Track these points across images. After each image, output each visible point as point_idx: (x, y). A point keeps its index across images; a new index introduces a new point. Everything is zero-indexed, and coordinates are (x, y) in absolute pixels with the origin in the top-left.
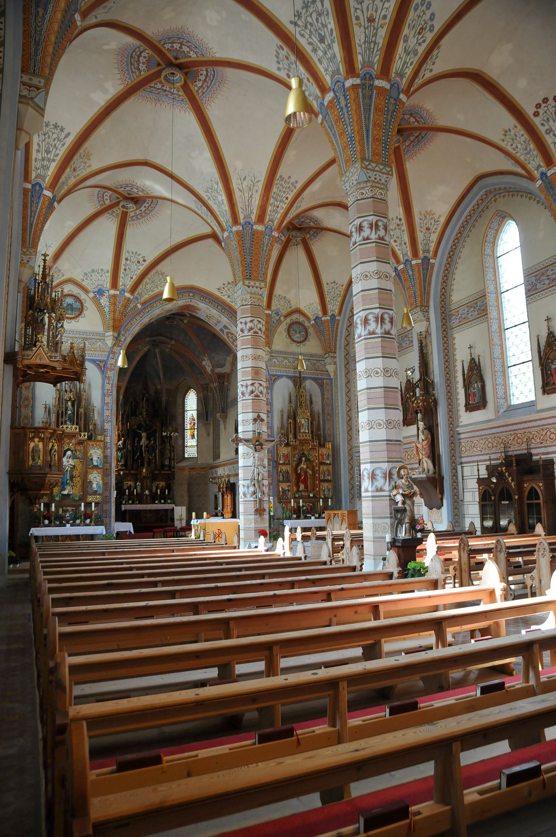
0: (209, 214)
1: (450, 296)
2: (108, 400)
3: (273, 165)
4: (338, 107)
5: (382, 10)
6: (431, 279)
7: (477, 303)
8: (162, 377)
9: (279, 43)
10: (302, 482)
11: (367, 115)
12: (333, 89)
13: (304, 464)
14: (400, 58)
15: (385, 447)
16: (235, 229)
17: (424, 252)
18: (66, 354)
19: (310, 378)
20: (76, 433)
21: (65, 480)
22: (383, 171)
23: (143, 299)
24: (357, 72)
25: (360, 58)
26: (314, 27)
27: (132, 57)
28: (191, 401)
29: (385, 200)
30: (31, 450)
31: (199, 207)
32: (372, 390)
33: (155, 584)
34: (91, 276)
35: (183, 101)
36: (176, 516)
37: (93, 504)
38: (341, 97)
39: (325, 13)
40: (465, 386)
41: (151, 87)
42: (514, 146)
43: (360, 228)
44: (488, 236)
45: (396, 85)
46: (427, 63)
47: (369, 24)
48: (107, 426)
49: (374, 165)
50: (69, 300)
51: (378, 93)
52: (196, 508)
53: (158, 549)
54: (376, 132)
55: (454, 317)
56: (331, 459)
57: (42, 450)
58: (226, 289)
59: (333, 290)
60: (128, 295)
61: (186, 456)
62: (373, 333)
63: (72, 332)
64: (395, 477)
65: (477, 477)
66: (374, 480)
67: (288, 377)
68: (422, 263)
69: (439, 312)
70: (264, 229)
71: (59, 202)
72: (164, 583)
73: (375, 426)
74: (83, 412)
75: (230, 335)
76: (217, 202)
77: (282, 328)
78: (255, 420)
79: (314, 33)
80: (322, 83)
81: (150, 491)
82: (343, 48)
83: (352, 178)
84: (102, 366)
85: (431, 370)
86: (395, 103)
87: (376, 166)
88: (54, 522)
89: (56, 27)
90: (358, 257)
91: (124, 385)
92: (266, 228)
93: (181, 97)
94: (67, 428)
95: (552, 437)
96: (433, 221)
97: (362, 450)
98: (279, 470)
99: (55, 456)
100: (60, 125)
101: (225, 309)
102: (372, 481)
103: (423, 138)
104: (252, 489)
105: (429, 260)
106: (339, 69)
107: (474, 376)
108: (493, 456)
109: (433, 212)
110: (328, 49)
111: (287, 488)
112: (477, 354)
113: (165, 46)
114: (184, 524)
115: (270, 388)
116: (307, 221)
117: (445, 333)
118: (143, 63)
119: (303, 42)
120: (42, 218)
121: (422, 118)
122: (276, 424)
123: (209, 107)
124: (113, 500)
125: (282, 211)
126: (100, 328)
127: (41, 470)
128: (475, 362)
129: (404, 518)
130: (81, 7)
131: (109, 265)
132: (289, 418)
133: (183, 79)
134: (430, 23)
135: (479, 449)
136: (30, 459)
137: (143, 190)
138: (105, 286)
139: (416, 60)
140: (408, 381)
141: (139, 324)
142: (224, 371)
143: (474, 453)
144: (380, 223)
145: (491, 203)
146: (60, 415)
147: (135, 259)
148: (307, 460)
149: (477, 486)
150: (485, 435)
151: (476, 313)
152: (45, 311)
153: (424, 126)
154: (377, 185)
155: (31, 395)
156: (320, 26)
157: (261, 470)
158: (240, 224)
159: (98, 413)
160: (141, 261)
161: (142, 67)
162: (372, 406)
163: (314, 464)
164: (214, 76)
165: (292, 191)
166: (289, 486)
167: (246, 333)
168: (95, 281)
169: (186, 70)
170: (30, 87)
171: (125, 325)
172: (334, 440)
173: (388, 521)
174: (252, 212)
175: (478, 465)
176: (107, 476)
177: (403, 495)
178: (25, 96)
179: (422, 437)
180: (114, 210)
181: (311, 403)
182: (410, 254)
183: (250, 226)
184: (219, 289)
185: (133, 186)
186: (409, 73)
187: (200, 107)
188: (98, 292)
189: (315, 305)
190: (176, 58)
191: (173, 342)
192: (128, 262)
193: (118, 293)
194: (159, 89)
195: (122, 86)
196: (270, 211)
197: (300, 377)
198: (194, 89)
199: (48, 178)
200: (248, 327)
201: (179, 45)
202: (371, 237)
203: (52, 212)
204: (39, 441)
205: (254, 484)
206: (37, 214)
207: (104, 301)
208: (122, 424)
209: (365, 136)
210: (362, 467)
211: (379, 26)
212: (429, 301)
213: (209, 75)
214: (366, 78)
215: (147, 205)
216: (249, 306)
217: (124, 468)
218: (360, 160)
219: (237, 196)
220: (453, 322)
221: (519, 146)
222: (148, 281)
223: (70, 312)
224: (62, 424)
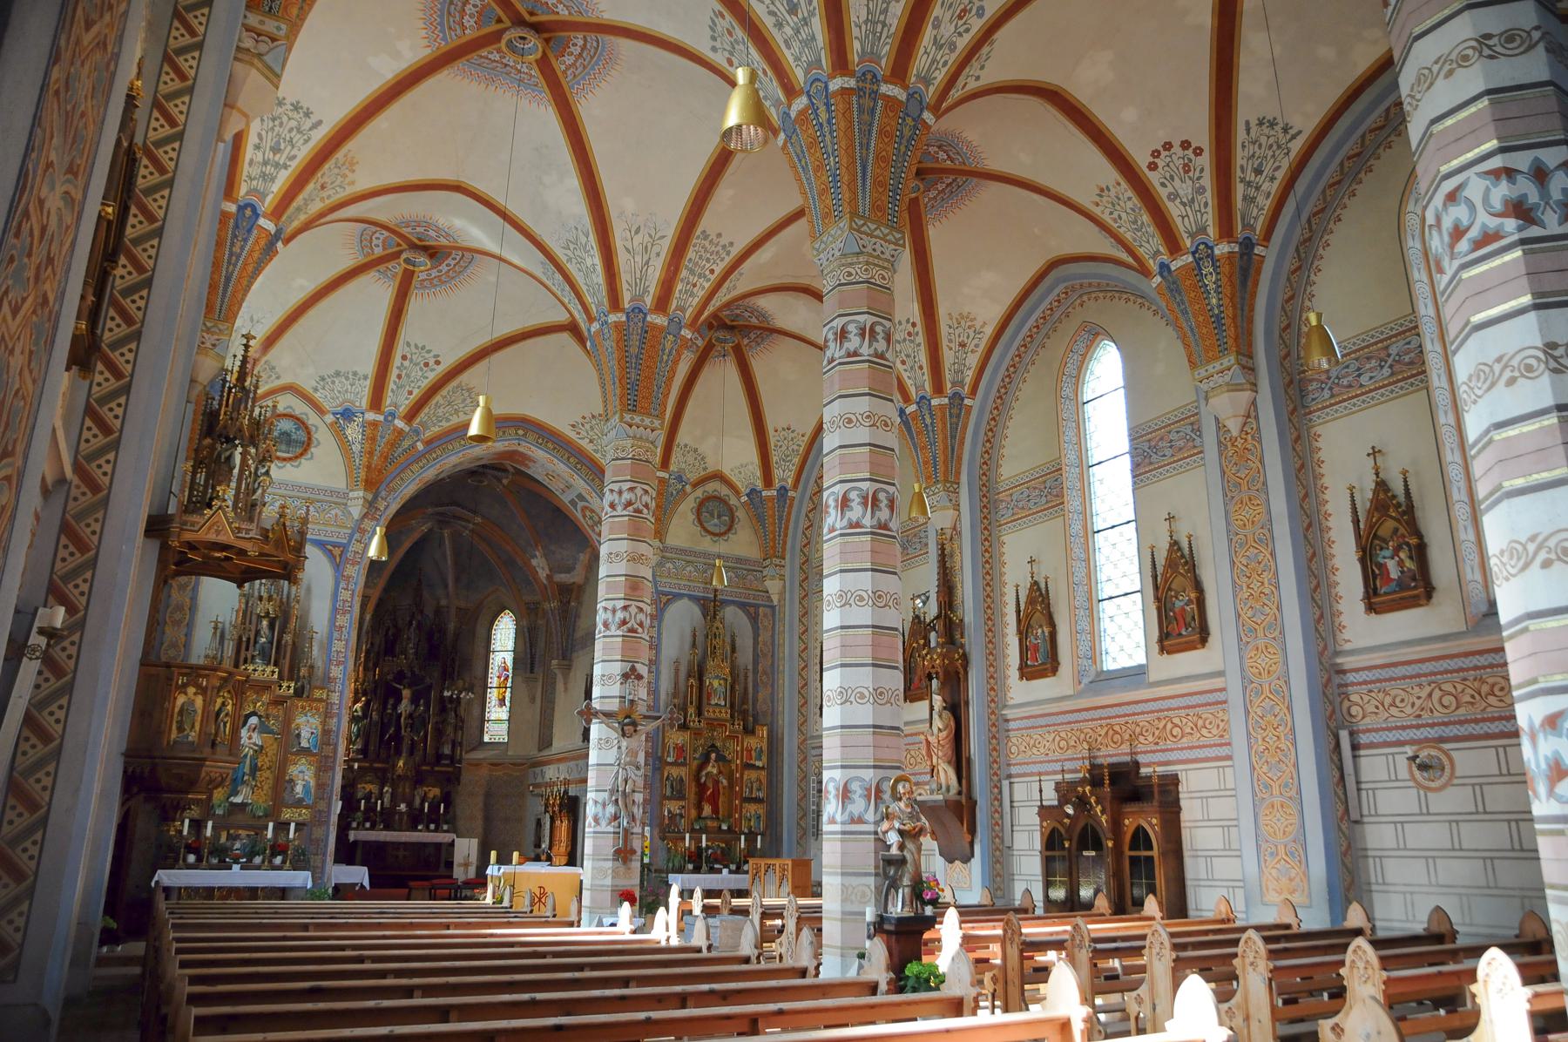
0: (567, 288)
10: (708, 801)
15: (869, 739)
16: (612, 318)
17: (954, 384)
23: (428, 434)
25: (857, 45)
28: (504, 634)
36: (458, 858)
37: (293, 826)
40: (1020, 632)
42: (1115, 215)
48: (336, 672)
50: (286, 425)
53: (417, 920)
56: (764, 758)
58: (587, 426)
60: (399, 423)
64: (887, 796)
67: (691, 597)
71: (287, 241)
77: (687, 506)
78: (625, 676)
81: (410, 805)
84: (337, 554)
91: (375, 595)
95: (1446, 700)
96: (971, 332)
104: (611, 809)
108: (1068, 766)
114: (472, 873)
118: (471, 16)
120: (250, 268)
122: (665, 685)
123: (583, 101)
124: (334, 819)
126: (340, 483)
128: (1039, 589)
129: (901, 877)
131: (369, 367)
132: (689, 676)
143: (1034, 758)
144: (878, 329)
148: (721, 758)
149: (1037, 820)
158: (623, 310)
159: (321, 647)
160: (431, 362)
161: (469, 22)
162: (848, 660)
169: (546, 35)
170: (259, 35)
173: (871, 881)
174: (646, 290)
177: (901, 832)
182: (928, 386)
185: (428, 225)
190: (532, 14)
191: (479, 520)
192: (406, 363)
193: (381, 418)
195: (428, 51)
198: (559, 66)
207: (353, 432)
210: (826, 775)
219: (622, 259)
221: (1124, 215)
223: (283, 447)
224: (245, 662)
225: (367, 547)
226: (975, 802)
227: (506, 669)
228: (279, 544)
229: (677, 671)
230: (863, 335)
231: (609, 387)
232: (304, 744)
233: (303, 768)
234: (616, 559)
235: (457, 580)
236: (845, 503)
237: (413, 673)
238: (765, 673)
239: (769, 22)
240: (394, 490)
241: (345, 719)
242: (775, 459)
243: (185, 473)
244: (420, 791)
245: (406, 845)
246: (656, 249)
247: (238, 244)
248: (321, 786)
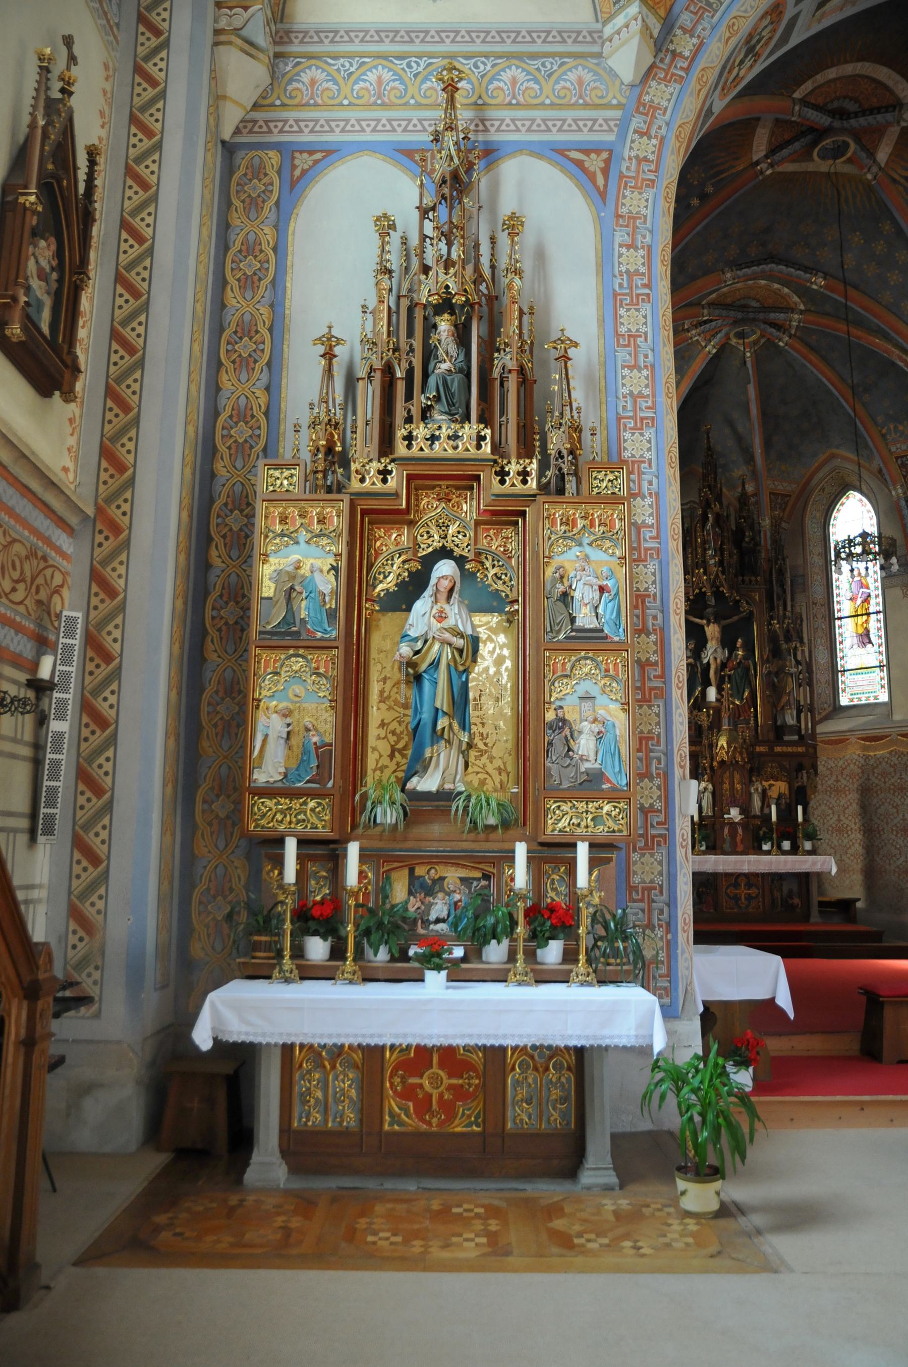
2: (631, 320)
8: (758, 451)
37: (582, 851)
48: (635, 445)
61: (844, 701)
88: (359, 954)
94: (433, 438)
146: (401, 387)
159: (590, 380)
235: (768, 444)
237: (718, 595)
244: (757, 787)
248: (643, 742)
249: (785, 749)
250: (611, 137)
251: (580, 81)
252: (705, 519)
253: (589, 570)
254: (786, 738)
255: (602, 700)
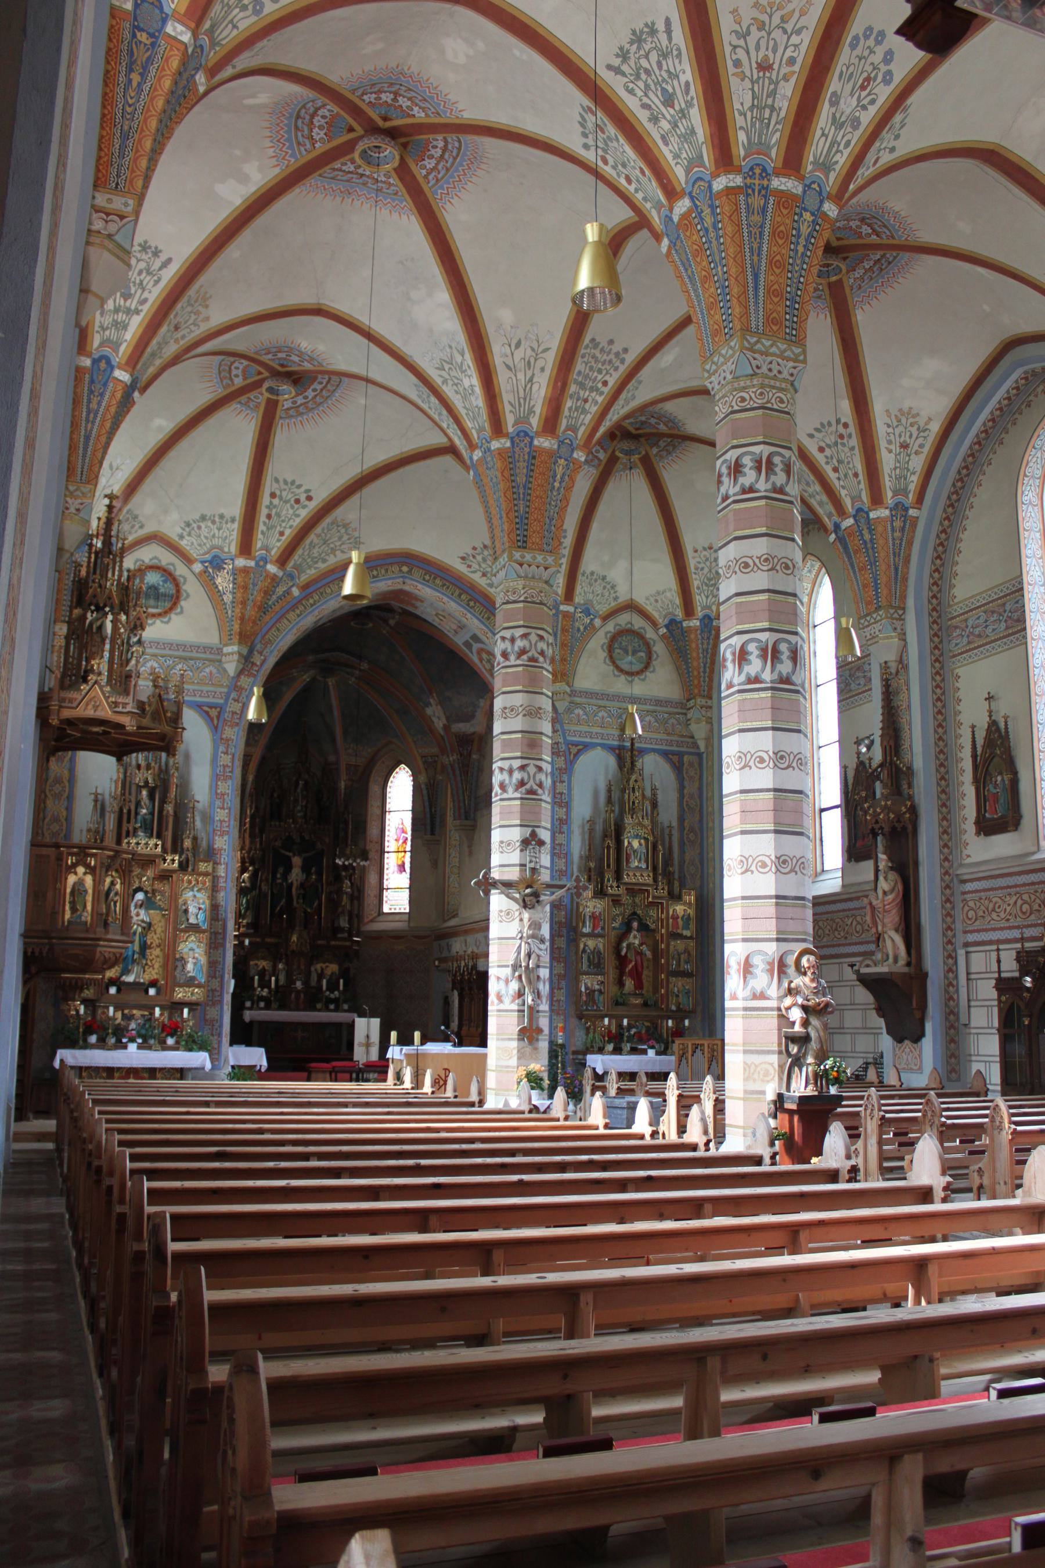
0: (445, 412)
1: (952, 586)
3: (568, 342)
4: (699, 227)
5: (786, 48)
6: (910, 550)
7: (1004, 604)
9: (587, 102)
11: (755, 246)
12: (690, 194)
13: (635, 937)
14: (823, 134)
15: (771, 911)
16: (495, 445)
17: (896, 493)
18: (145, 700)
19: (654, 750)
20: (157, 856)
21: (130, 953)
22: (786, 354)
23: (304, 578)
24: (736, 163)
25: (742, 136)
26: (653, 77)
27: (298, 117)
28: (400, 790)
29: (788, 413)
30: (68, 890)
31: (425, 396)
32: (751, 796)
33: (306, 1157)
34: (199, 528)
35: (396, 194)
36: (359, 1036)
38: (704, 208)
39: (675, 53)
40: (976, 781)
41: (334, 170)
43: (737, 469)
44: (1031, 464)
45: (815, 186)
46: (883, 139)
47: (761, 74)
49: (768, 343)
50: (152, 578)
51: (779, 203)
52: (401, 1024)
53: (318, 1100)
54: (772, 278)
55: (958, 631)
56: (692, 925)
57: (90, 891)
58: (479, 558)
59: (708, 563)
60: (272, 568)
62: (757, 680)
63: (156, 643)
64: (791, 971)
65: (996, 975)
66: (749, 976)
67: (603, 746)
68: (892, 515)
69: (926, 621)
70: (556, 447)
71: (143, 390)
72: (322, 1156)
73: (753, 868)
74: (171, 812)
75: (484, 656)
76: (461, 389)
77: (597, 643)
78: (525, 843)
79: (653, 87)
80: (669, 181)
81: (306, 983)
82: (709, 119)
83: (725, 367)
84: (214, 716)
85: (906, 745)
86: (813, 221)
87: (772, 346)
89: (160, 103)
90: (731, 527)
91: (257, 753)
92: (561, 443)
93: (392, 188)
94: (138, 844)
96: (914, 430)
97: (728, 914)
98: (582, 946)
99: (115, 903)
100: (153, 245)
101: (476, 601)
102: (745, 978)
103: (890, 263)
104: (514, 986)
105: (906, 510)
106: (702, 157)
107: (996, 760)
108: (1028, 933)
109: (914, 412)
110: (680, 118)
111: (597, 987)
112: (1002, 714)
113: (365, 97)
114: (374, 1056)
115: (563, 773)
116: (653, 421)
117: (937, 664)
118: (321, 128)
119: (632, 104)
120: (108, 424)
121: (885, 226)
122: (577, 847)
123: (448, 206)
124: (228, 998)
125: (594, 409)
126: (212, 637)
127: (87, 931)
128: (998, 729)
129: (805, 1055)
130: (207, 61)
131: (235, 508)
132: (605, 835)
133: (398, 157)
134: (883, 68)
135: (1002, 915)
136: (67, 907)
137: (312, 359)
138: (226, 550)
139: (856, 137)
140: (861, 764)
141: (294, 631)
142: (472, 730)
143: (993, 924)
144: (777, 460)
145: (1036, 396)
147: (290, 496)
148: (644, 928)
149: (994, 994)
150: (1016, 886)
151: (1003, 625)
152: (107, 609)
153: (891, 242)
154: (772, 383)
155: (66, 772)
156: (665, 76)
157: (535, 944)
158: (507, 435)
160: (303, 498)
161: (318, 134)
162: (749, 827)
163: (658, 937)
164: (459, 149)
165: (616, 369)
166: (602, 982)
167: (513, 660)
168: (206, 538)
169: (403, 140)
170: (108, 214)
171: (264, 630)
172: (701, 887)
173: (774, 1059)
174: (531, 411)
175: (998, 950)
176: (216, 948)
177: (805, 1008)
178: (99, 232)
179: (883, 885)
180: (252, 395)
181: (655, 805)
182: (865, 497)
183: (527, 440)
184: (463, 558)
185: (290, 350)
186: (842, 161)
187: (431, 207)
188: (211, 562)
189: (668, 594)
190: (385, 119)
191: (365, 666)
192: (276, 501)
193: (252, 564)
194: (349, 172)
195: (277, 170)
196: (570, 409)
197: (632, 749)
198: (419, 173)
199: (124, 345)
200: (516, 648)
201: (392, 96)
202: (757, 486)
203: (128, 411)
204: (85, 874)
205: (520, 977)
206: (99, 416)
207: (223, 581)
208: (250, 836)
209: (751, 285)
210: (728, 948)
211: (781, 76)
212: (905, 597)
213: (450, 147)
214: (754, 174)
215: (319, 387)
216: (521, 605)
217: (252, 931)
218: (739, 333)
219: (503, 379)
220: (954, 642)
222: (316, 541)
223: (152, 602)
224: (128, 835)
225: (245, 707)
226: (926, 975)
227: (404, 831)
228: (156, 716)
229: (591, 831)
230: (759, 469)
231: (496, 522)
232: (192, 920)
233: (193, 945)
234: (510, 716)
236: (742, 657)
238: (692, 830)
239: (643, 116)
240: (270, 642)
241: (233, 892)
242: (696, 583)
243: (61, 647)
245: (304, 1026)
246: (540, 363)
247: (95, 400)
249: (338, 943)
250: (222, 701)
251: (211, 673)
252: (297, 784)
253: (195, 903)
254: (340, 936)
255: (197, 950)
